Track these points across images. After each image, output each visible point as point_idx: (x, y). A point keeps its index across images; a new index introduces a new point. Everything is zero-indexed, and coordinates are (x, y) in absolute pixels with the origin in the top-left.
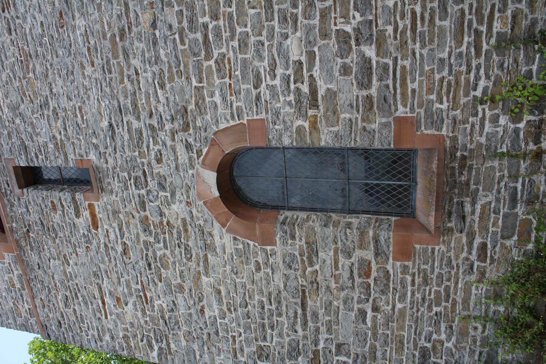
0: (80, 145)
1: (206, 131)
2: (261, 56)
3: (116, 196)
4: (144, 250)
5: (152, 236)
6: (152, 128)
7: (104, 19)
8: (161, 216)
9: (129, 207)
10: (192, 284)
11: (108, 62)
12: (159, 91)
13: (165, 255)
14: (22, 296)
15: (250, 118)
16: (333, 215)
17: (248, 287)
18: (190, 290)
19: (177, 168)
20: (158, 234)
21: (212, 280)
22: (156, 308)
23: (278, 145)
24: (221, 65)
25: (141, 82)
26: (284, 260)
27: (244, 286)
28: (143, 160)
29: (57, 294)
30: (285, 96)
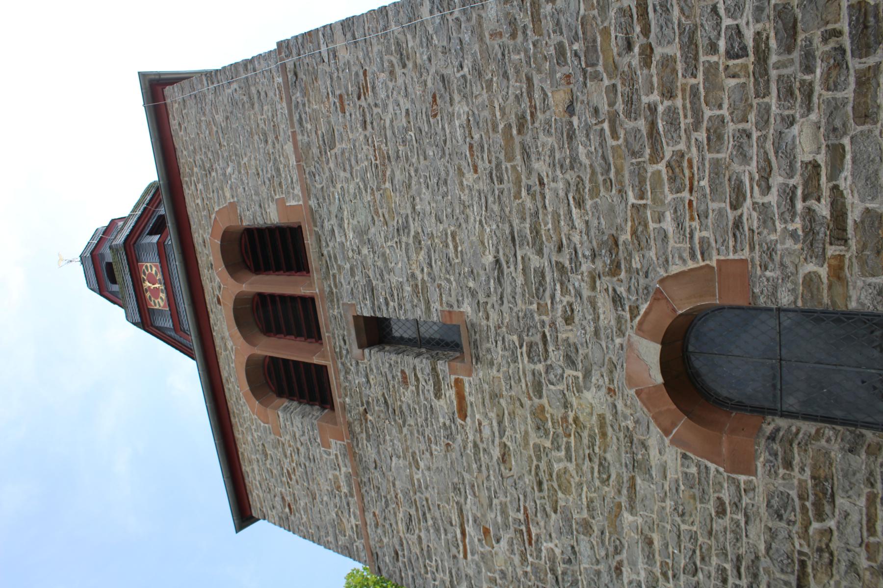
0: (450, 290)
1: (646, 277)
2: (745, 156)
3: (498, 371)
4: (534, 458)
5: (548, 439)
6: (561, 268)
7: (496, 101)
8: (566, 407)
9: (516, 389)
10: (606, 523)
11: (498, 165)
12: (574, 211)
13: (566, 471)
14: (348, 504)
15: (722, 258)
16: (869, 434)
17: (700, 540)
18: (602, 533)
19: (597, 333)
20: (558, 436)
21: (640, 520)
22: (544, 553)
23: (770, 305)
24: (677, 170)
25: (547, 197)
26: (769, 502)
27: (693, 537)
28: (544, 318)
29: (397, 510)
30: (786, 222)
